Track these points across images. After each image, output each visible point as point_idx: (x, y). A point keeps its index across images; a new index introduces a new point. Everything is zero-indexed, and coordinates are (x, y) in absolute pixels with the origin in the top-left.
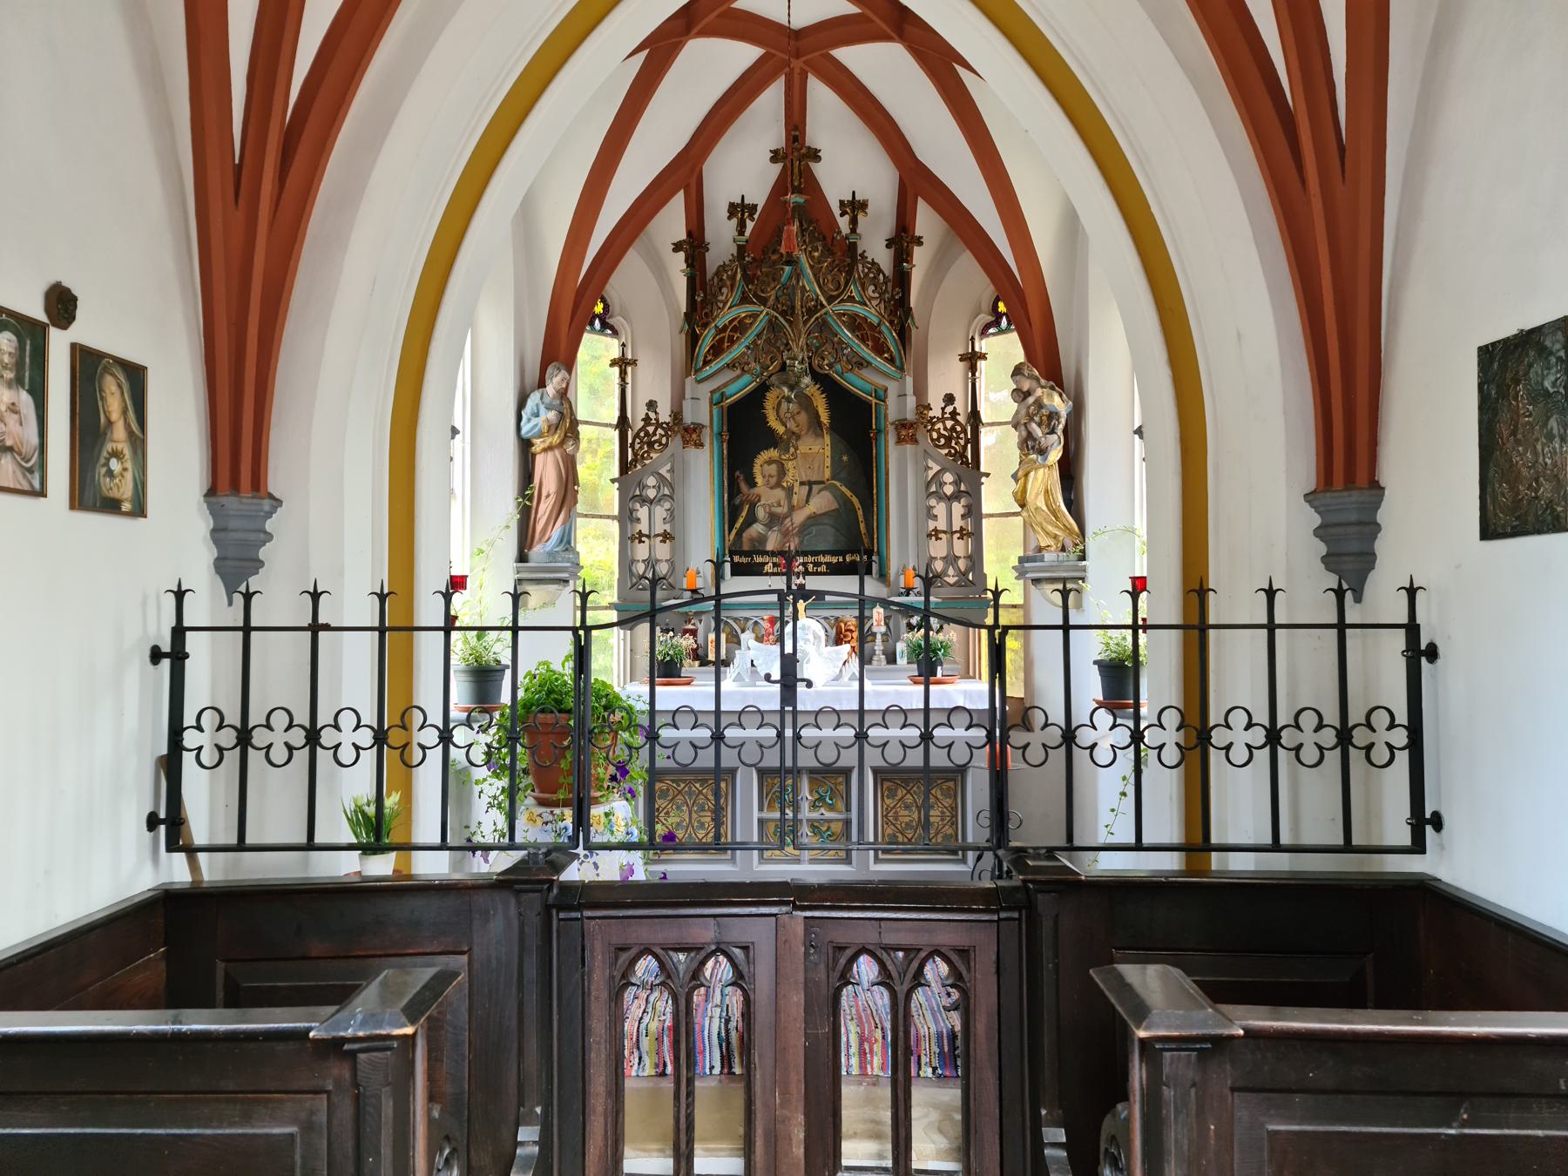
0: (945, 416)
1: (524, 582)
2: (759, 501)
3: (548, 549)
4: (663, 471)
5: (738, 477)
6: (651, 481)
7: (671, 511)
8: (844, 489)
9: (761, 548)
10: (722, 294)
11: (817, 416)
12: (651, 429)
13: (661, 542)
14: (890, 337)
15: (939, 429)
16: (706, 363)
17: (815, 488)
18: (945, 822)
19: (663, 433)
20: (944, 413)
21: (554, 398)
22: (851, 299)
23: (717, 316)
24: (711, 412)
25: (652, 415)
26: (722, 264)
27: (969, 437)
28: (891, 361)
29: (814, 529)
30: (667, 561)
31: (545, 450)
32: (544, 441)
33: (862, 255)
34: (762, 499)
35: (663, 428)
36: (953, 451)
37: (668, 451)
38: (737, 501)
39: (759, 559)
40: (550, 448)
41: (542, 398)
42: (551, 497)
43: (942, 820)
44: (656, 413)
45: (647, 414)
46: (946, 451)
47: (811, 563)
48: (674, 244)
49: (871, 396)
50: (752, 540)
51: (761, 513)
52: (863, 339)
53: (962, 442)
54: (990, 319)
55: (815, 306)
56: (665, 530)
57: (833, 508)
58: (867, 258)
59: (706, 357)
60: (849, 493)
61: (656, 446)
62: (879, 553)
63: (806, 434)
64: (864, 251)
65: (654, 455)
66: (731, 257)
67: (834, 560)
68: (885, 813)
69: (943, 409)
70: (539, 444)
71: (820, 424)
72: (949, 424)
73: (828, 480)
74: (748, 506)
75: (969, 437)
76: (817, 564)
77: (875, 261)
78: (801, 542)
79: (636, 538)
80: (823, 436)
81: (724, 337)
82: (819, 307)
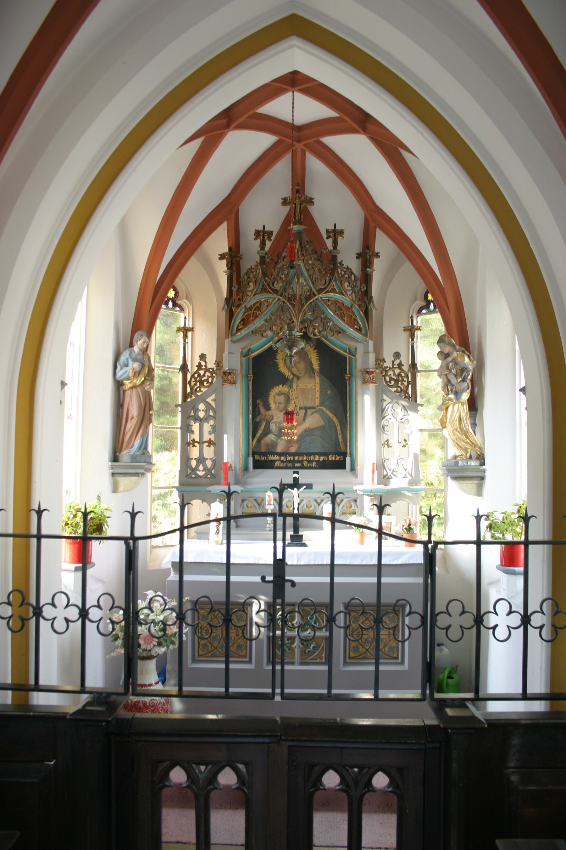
0: (395, 366)
1: (115, 475)
2: (272, 419)
3: (132, 453)
4: (209, 400)
5: (259, 403)
6: (202, 406)
7: (214, 427)
8: (328, 412)
9: (273, 451)
10: (250, 287)
11: (311, 364)
12: (202, 372)
13: (207, 446)
14: (359, 315)
15: (391, 374)
16: (238, 330)
17: (309, 411)
18: (390, 639)
19: (210, 375)
20: (393, 364)
21: (138, 354)
22: (333, 291)
23: (246, 300)
24: (241, 361)
25: (203, 363)
26: (250, 267)
27: (410, 380)
28: (359, 330)
29: (308, 439)
30: (211, 459)
31: (131, 388)
32: (131, 383)
33: (341, 263)
34: (274, 418)
35: (210, 372)
36: (399, 389)
37: (213, 387)
38: (258, 419)
39: (272, 458)
40: (134, 387)
41: (130, 354)
42: (134, 419)
43: (389, 637)
44: (205, 362)
45: (200, 363)
46: (395, 389)
47: (306, 460)
48: (220, 255)
49: (346, 352)
50: (267, 445)
51: (273, 427)
52: (342, 317)
53: (405, 384)
54: (424, 304)
55: (310, 295)
56: (210, 439)
57: (321, 425)
58: (343, 265)
59: (238, 326)
60: (331, 415)
61: (205, 383)
62: (351, 456)
63: (304, 376)
64: (342, 261)
65: (204, 390)
66: (256, 264)
67: (321, 459)
68: (351, 633)
69: (393, 362)
70: (128, 384)
71: (313, 370)
72: (397, 371)
73: (318, 406)
74: (265, 423)
75: (410, 380)
76: (310, 461)
77: (349, 267)
78: (299, 447)
79: (192, 444)
80: (315, 377)
81: (251, 313)
82: (312, 296)
